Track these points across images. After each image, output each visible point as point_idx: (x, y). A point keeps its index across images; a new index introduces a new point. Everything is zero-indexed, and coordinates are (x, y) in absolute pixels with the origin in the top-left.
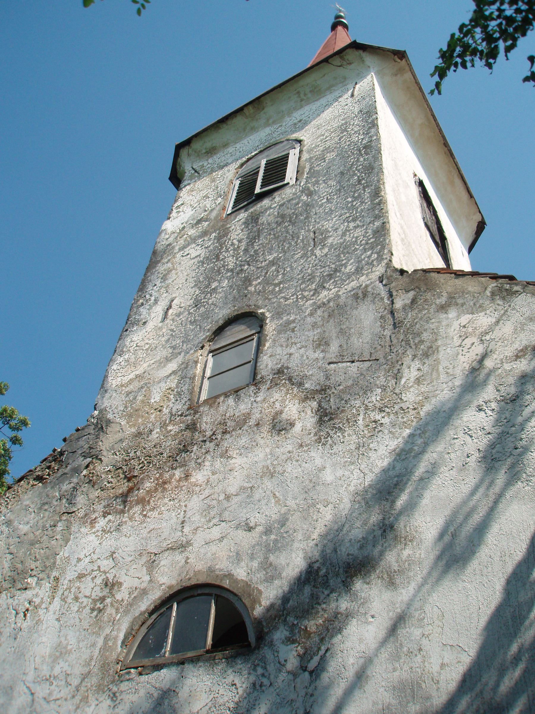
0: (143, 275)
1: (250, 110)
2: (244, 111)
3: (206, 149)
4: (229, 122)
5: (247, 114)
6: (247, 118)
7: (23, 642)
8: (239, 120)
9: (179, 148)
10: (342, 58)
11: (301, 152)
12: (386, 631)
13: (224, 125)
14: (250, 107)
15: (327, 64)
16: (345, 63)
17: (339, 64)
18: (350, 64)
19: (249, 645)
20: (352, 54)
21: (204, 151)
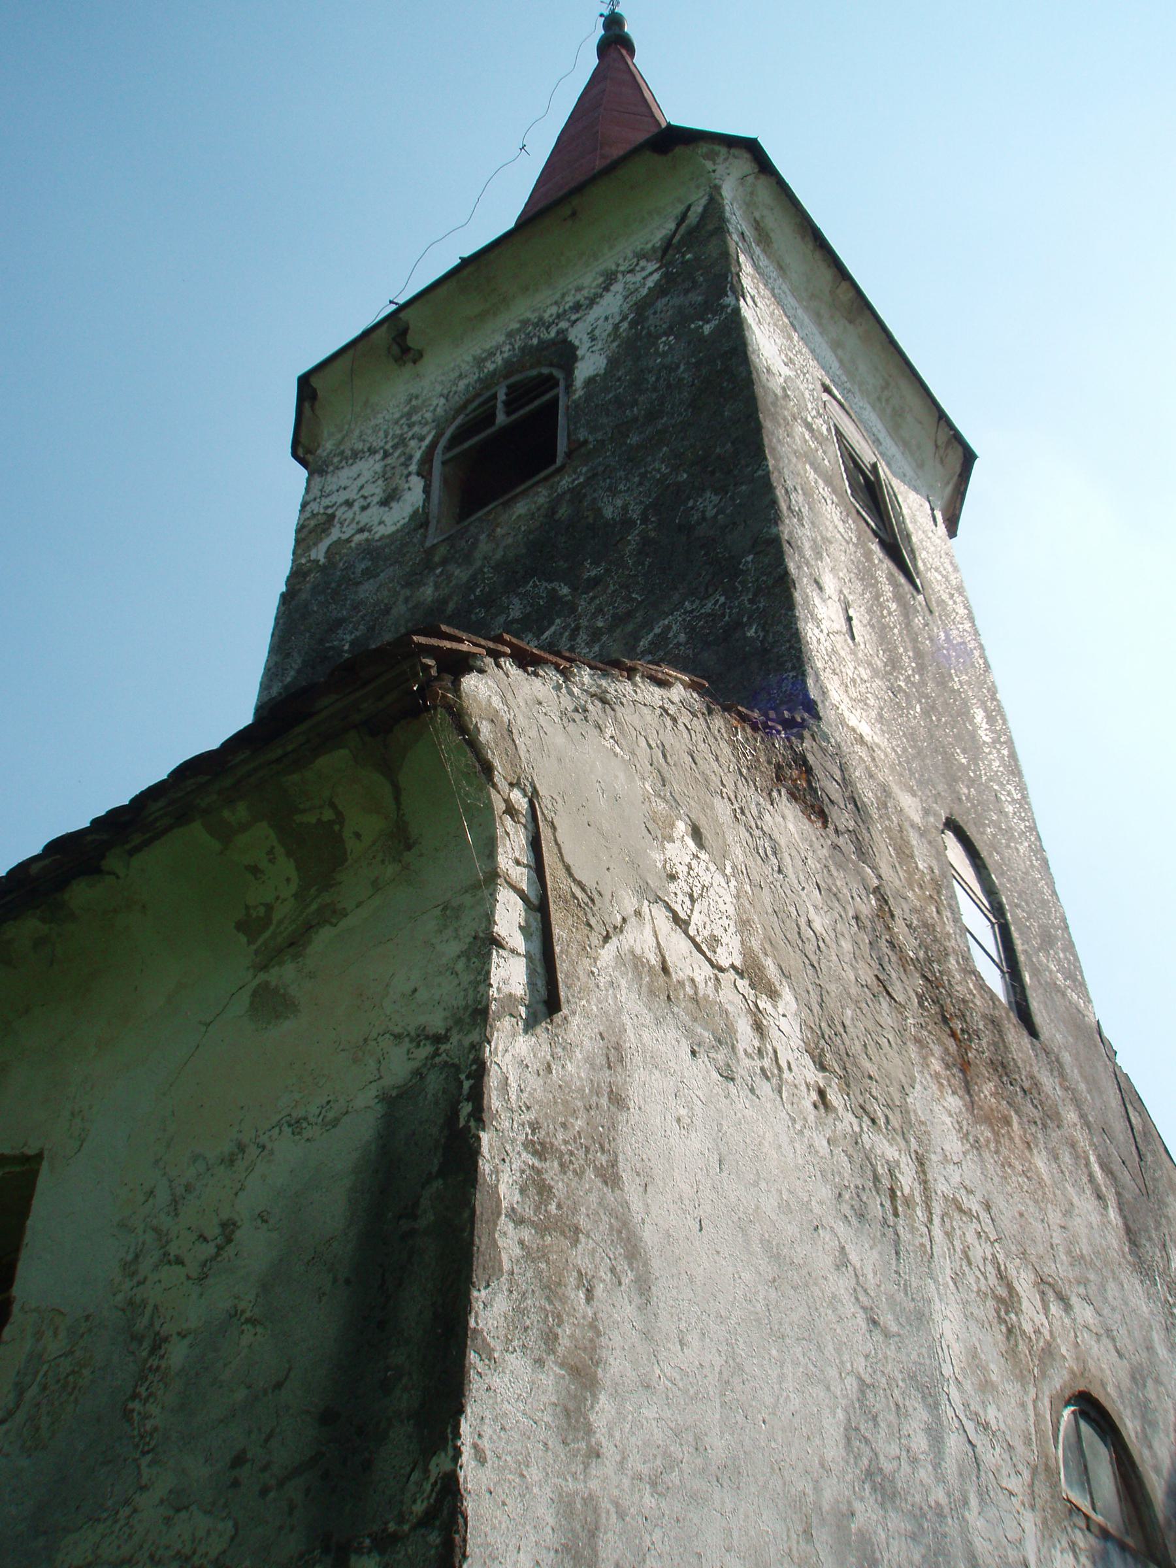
0: (986, 646)
1: (844, 295)
2: (843, 283)
3: (763, 217)
4: (818, 255)
5: (839, 291)
6: (832, 292)
7: (785, 658)
8: (826, 275)
9: (752, 148)
10: (949, 443)
11: (809, 426)
12: (718, 722)
13: (811, 246)
14: (852, 293)
15: (936, 419)
16: (942, 451)
17: (939, 443)
18: (942, 462)
19: (634, 647)
20: (955, 460)
21: (757, 215)
